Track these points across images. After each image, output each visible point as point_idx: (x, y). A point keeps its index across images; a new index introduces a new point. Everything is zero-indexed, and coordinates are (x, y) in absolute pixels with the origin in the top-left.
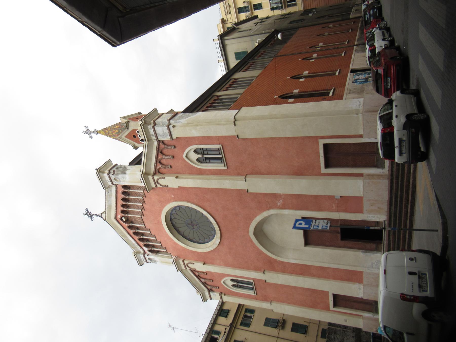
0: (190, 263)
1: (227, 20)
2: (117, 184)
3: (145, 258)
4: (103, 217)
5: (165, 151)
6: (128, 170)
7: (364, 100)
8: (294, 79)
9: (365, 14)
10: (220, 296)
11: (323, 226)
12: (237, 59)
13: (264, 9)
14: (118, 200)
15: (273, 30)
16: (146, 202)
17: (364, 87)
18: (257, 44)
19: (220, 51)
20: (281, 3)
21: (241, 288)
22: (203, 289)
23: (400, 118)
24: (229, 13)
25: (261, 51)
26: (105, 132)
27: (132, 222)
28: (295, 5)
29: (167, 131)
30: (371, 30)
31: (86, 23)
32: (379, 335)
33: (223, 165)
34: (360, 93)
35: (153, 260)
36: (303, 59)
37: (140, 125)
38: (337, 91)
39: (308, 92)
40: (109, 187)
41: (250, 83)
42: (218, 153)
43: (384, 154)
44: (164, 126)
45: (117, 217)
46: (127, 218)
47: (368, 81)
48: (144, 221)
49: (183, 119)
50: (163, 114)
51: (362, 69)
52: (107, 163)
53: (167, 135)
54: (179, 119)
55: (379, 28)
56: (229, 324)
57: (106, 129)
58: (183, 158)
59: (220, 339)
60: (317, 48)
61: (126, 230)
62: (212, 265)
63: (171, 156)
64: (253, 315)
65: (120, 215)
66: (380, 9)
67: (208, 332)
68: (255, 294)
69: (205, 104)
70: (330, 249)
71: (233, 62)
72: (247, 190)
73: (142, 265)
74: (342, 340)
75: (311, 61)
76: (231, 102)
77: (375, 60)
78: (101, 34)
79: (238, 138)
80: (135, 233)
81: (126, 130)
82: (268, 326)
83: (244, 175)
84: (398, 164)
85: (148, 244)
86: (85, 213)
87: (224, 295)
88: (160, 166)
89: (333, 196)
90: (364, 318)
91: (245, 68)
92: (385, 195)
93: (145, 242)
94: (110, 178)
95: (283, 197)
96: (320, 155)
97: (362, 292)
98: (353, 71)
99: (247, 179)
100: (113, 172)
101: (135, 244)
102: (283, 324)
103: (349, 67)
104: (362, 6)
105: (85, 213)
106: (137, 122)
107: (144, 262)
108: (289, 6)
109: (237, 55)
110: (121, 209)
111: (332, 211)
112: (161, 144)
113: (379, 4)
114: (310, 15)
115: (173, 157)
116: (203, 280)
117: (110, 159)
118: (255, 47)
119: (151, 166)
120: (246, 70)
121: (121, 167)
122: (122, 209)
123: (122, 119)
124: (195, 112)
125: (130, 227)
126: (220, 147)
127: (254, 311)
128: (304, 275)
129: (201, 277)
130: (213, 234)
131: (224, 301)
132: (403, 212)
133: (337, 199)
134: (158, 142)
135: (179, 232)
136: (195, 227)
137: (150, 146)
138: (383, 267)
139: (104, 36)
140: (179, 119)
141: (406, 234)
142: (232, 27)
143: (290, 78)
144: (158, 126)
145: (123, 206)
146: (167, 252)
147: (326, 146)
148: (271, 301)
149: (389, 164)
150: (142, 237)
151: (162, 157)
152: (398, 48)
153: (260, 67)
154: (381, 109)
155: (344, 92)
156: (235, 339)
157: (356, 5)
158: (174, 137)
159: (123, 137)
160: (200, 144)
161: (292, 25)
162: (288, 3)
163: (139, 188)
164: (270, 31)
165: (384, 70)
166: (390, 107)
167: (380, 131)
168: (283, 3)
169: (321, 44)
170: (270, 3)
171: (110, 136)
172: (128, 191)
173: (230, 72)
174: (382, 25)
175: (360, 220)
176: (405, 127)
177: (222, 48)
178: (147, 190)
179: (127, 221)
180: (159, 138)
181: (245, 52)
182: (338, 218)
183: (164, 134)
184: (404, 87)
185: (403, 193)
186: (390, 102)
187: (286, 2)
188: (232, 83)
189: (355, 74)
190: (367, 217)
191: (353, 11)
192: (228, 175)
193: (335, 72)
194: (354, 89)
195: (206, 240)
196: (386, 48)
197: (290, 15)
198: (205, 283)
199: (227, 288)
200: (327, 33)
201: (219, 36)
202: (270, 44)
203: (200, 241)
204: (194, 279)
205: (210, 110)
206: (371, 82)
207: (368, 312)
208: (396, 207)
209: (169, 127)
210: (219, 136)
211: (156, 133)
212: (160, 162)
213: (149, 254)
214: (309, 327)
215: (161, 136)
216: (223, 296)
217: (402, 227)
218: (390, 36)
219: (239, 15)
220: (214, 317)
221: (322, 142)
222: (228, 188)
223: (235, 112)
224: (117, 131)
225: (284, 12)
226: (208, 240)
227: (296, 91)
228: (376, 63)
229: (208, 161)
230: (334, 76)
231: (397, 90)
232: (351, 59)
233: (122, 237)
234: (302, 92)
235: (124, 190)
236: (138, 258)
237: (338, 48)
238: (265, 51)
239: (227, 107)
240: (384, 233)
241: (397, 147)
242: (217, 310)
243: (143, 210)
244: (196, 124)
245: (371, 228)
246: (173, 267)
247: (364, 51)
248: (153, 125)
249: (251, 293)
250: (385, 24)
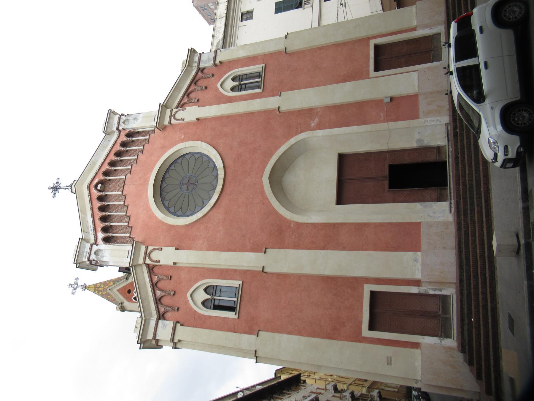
10: (174, 326)
97: (420, 268)
110: (98, 204)
190: (424, 122)
204: (146, 290)
221: (372, 43)
236: (81, 246)
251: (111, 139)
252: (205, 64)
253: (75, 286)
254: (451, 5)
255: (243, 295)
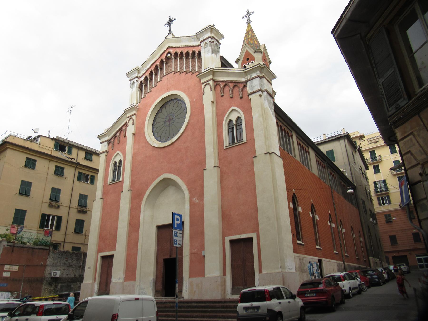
0: (133, 121)
1: (363, 140)
2: (201, 46)
3: (134, 79)
4: (169, 35)
5: (236, 89)
6: (216, 55)
7: (294, 273)
8: (311, 206)
9: (373, 271)
10: (105, 152)
11: (176, 240)
12: (327, 152)
13: (374, 175)
14: (187, 48)
15: (355, 185)
16: (187, 75)
17: (305, 272)
18: (342, 170)
19: (333, 136)
20: (381, 191)
21: (114, 170)
22: (110, 135)
23: (279, 306)
24: (369, 142)
25: (336, 175)
26: (250, 31)
27: (167, 63)
28: (380, 204)
29: (255, 89)
30: (359, 277)
31: (353, 2)
32: (78, 299)
33: (228, 145)
34: (301, 269)
35: (133, 86)
36: (330, 214)
37: (259, 63)
38: (302, 248)
39: (300, 220)
40: (198, 39)
41: (306, 166)
42: (238, 140)
43: (245, 293)
44: (260, 87)
45: (171, 49)
46: (171, 58)
47: (312, 276)
48: (169, 74)
49: (268, 103)
50: (271, 84)
51: (322, 270)
52: (221, 35)
53: (252, 90)
54: (267, 100)
55: (361, 284)
56: (78, 161)
57: (252, 31)
58: (232, 107)
59: (64, 154)
60: (340, 228)
61: (158, 58)
62: (133, 142)
63: (232, 95)
64: (89, 183)
65: (173, 51)
66: (378, 284)
67: (70, 143)
68: (109, 183)
69: (284, 124)
70: (155, 249)
71: (324, 149)
72: (206, 169)
73: (127, 76)
74: (71, 266)
75: (329, 222)
76: (287, 148)
77: (331, 281)
78: (343, 18)
79: (253, 157)
80: (157, 67)
81: (254, 51)
82: (80, 198)
83: (219, 165)
84: (236, 307)
85: (148, 80)
86: (171, 18)
87: (105, 155)
88: (222, 86)
89: (204, 250)
90: (93, 284)
91: (319, 160)
92: (207, 297)
93: (149, 77)
94: (207, 38)
95: (201, 203)
96: (242, 235)
97: (116, 281)
98: (320, 261)
99: (216, 168)
100: (213, 41)
101: (147, 68)
102: (82, 211)
103: (324, 258)
104: (381, 267)
105: (171, 18)
106: (261, 60)
107: (130, 78)
108: (378, 199)
109: (331, 152)
111: (190, 250)
112: (243, 85)
113: (383, 284)
114: (371, 219)
115: (232, 97)
116: (118, 134)
117: (224, 37)
118: (339, 169)
119: (221, 77)
120: (317, 161)
121: (218, 48)
122: (179, 53)
123: (264, 46)
124: (275, 115)
125: (162, 61)
126: (244, 141)
127: (93, 184)
128: (129, 227)
129: (121, 132)
130: (162, 141)
131: (100, 155)
132: (192, 314)
133: (202, 252)
134: (245, 82)
135: (161, 108)
136: (167, 123)
137: (240, 74)
138: (142, 298)
139: (341, 21)
140: (268, 100)
141: (172, 317)
142: (357, 146)
143: (311, 204)
144: (260, 80)
145: (182, 53)
146: (142, 98)
147: (250, 240)
148: (103, 199)
149: (236, 299)
150: (154, 74)
151: (231, 87)
152: (342, 302)
153: (320, 173)
154: (286, 289)
155: (300, 254)
156: (65, 168)
157: (382, 262)
158: (250, 97)
159: (247, 49)
160: (245, 122)
161: (361, 202)
162: (381, 198)
163: (200, 67)
164: (355, 182)
165: (322, 290)
166: (288, 297)
167: (266, 288)
168: (381, 193)
169: (344, 230)
170: (381, 181)
171: (246, 36)
172: (196, 57)
173: (315, 147)
174: (364, 287)
175: (183, 275)
176: (271, 311)
177: (337, 137)
178: (198, 75)
179: (168, 59)
180: (249, 82)
181: (334, 159)
182: (184, 255)
183: (252, 87)
184: (306, 310)
185: (210, 313)
186: (293, 297)
187: (382, 196)
188: (304, 149)
189: (317, 263)
191: (376, 259)
192: (218, 149)
193: (319, 245)
194: (304, 263)
195: (156, 134)
196: (343, 291)
197: (370, 200)
198: (116, 136)
199: (112, 157)
200: (354, 236)
201: (347, 134)
202: (343, 183)
203: (155, 129)
204: (119, 126)
205: (278, 129)
206: (310, 279)
207: (98, 287)
208: (196, 307)
209: (259, 91)
210: (254, 139)
211: (253, 79)
212: (226, 85)
213: (138, 82)
214: (82, 235)
215: (250, 84)
216: (105, 154)
217: (178, 314)
218: (354, 295)
219: (368, 152)
220: (84, 148)
221: (254, 235)
222: (207, 151)
223: (278, 153)
224: (252, 42)
225: (373, 194)
226: (156, 136)
227: (300, 209)
228: (328, 282)
229: (230, 130)
230: (315, 244)
231: (304, 303)
232: (331, 259)
233: (152, 55)
234: (299, 215)
235: (196, 53)
237: (341, 247)
238: (336, 178)
239: (282, 146)
240: (172, 298)
241: (252, 305)
242: (91, 149)
243: (179, 73)
244: (264, 117)
245: (176, 284)
246: (128, 106)
247: (339, 271)
248: (261, 75)
249: (110, 180)
250: (364, 289)
251: (196, 41)
252: (249, 86)
253: (248, 15)
254: (215, 305)
255: (117, 183)
